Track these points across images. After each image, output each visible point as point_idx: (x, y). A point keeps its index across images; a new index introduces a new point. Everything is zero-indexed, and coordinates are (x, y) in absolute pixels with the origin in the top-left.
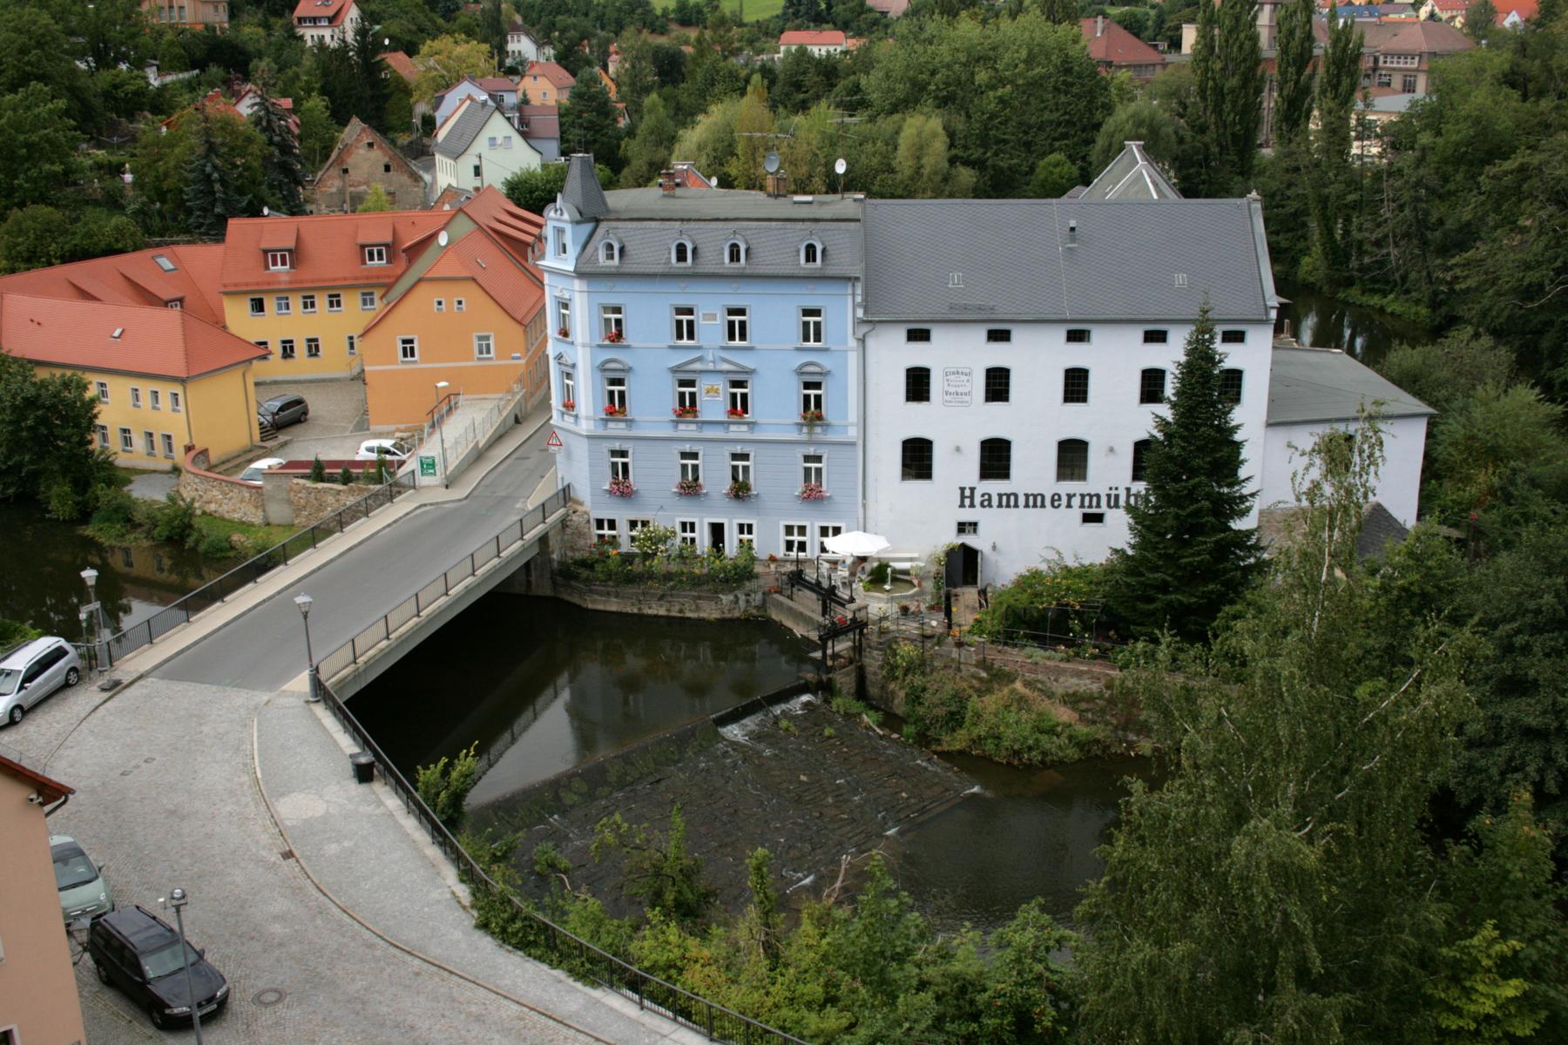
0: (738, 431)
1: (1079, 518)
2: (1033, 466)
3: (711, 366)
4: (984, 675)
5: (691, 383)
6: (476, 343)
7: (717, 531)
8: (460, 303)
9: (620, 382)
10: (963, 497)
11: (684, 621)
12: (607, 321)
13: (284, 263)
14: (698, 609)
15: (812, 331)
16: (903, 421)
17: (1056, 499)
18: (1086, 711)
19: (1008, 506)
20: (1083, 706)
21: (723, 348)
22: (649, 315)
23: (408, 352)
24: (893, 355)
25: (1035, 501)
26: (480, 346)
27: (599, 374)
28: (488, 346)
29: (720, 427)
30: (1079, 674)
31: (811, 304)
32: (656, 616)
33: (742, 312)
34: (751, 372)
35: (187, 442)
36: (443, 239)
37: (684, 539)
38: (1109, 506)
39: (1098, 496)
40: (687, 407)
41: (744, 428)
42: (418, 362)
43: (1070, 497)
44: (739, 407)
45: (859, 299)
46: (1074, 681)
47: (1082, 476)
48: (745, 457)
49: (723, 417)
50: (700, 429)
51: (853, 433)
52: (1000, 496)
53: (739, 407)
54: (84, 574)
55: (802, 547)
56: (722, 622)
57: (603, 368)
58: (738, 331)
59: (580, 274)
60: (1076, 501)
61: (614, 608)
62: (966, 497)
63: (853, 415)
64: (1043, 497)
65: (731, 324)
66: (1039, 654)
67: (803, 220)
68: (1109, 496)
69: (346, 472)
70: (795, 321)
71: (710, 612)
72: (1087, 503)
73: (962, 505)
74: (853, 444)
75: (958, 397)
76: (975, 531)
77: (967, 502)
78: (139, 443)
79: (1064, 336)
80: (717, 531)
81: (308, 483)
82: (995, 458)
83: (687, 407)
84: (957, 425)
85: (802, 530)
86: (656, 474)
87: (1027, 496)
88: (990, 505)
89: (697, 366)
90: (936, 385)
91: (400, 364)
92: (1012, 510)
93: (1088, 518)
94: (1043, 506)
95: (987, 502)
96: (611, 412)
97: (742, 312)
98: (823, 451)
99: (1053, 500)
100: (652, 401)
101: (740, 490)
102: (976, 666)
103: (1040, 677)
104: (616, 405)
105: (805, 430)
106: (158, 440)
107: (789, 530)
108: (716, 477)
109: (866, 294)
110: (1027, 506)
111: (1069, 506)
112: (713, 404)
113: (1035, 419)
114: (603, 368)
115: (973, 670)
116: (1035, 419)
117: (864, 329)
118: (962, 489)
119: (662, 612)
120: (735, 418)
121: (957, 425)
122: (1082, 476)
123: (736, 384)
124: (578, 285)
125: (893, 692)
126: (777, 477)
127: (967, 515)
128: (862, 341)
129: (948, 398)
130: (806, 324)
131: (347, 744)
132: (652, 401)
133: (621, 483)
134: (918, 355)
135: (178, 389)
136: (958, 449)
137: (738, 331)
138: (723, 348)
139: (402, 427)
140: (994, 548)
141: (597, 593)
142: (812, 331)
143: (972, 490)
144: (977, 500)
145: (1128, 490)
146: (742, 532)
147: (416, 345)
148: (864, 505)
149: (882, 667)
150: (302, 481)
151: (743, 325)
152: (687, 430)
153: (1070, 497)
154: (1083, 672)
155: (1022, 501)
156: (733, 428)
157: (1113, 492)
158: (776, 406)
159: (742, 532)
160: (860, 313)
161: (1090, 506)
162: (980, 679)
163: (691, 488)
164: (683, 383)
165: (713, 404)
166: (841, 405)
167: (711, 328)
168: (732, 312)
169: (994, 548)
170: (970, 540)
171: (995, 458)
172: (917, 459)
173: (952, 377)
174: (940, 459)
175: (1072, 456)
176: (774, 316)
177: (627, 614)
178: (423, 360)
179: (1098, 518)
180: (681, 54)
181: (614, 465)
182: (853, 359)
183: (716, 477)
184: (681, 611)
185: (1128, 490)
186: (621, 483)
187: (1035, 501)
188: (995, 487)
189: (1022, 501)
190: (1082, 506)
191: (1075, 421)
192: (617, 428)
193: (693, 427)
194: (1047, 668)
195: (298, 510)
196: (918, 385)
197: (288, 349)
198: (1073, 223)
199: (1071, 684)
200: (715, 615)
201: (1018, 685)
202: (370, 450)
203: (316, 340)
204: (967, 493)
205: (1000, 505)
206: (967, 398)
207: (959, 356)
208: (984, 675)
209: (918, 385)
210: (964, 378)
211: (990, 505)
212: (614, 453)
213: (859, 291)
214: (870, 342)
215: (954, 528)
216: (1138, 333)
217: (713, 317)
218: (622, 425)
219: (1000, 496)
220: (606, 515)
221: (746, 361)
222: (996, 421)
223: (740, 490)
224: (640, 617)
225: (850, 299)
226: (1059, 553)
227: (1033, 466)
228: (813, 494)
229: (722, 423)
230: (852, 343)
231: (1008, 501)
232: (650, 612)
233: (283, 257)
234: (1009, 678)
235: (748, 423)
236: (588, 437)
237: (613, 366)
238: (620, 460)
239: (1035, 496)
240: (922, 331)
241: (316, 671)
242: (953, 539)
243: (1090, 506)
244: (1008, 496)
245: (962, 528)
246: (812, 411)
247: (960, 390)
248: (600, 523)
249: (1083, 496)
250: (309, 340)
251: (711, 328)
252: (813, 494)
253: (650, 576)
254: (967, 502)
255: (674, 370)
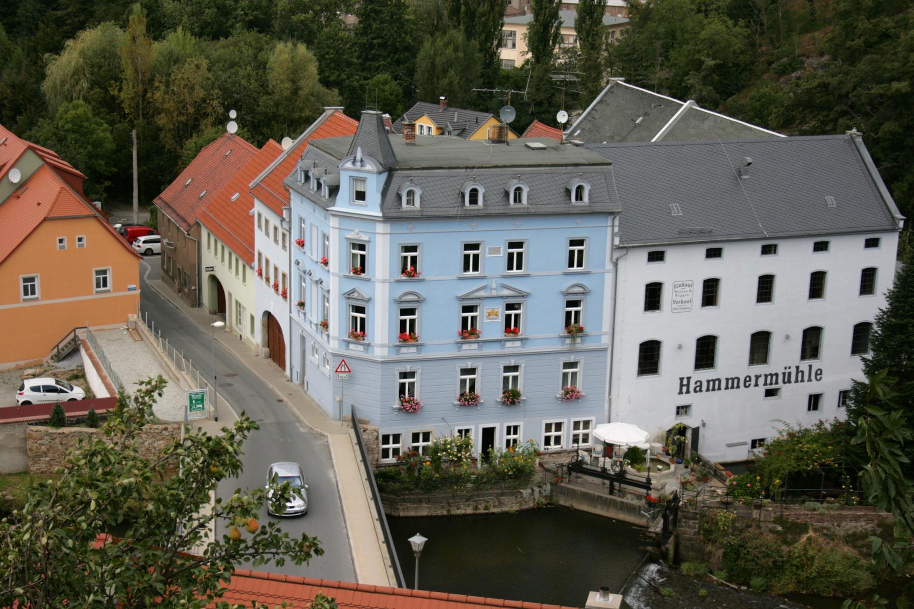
0: (513, 346)
1: (763, 393)
2: (732, 357)
3: (494, 293)
4: (780, 528)
7: (488, 435)
10: (682, 385)
11: (489, 516)
12: (354, 255)
14: (501, 504)
15: (575, 259)
16: (639, 326)
17: (748, 379)
18: (862, 546)
20: (860, 543)
21: (505, 277)
22: (441, 249)
23: (29, 290)
24: (638, 272)
25: (733, 383)
26: (98, 280)
27: (344, 301)
29: (498, 345)
30: (856, 519)
32: (465, 516)
34: (525, 295)
38: (784, 382)
40: (468, 329)
41: (518, 344)
43: (757, 377)
44: (511, 326)
45: (616, 229)
46: (853, 524)
50: (480, 348)
53: (511, 326)
55: (558, 440)
56: (522, 513)
57: (348, 295)
58: (514, 261)
59: (386, 219)
60: (761, 381)
61: (424, 513)
62: (684, 385)
63: (606, 327)
66: (821, 507)
67: (566, 165)
68: (784, 374)
69: (92, 414)
71: (511, 505)
72: (769, 382)
73: (681, 393)
74: (605, 350)
75: (681, 305)
77: (684, 389)
80: (488, 435)
81: (52, 430)
82: (706, 351)
83: (468, 329)
85: (559, 426)
86: (437, 390)
88: (701, 391)
89: (482, 294)
92: (716, 392)
93: (770, 393)
95: (699, 389)
96: (354, 335)
99: (745, 381)
100: (438, 325)
101: (512, 398)
102: (774, 522)
103: (826, 524)
104: (407, 332)
105: (568, 341)
108: (490, 387)
112: (490, 324)
114: (348, 295)
115: (771, 525)
117: (617, 254)
118: (682, 379)
119: (469, 511)
120: (511, 336)
121: (677, 328)
123: (509, 307)
124: (380, 228)
125: (710, 553)
126: (539, 384)
127: (684, 400)
129: (675, 306)
132: (438, 325)
133: (408, 403)
136: (680, 347)
137: (514, 261)
138: (505, 277)
141: (410, 501)
142: (575, 259)
143: (689, 379)
145: (797, 367)
147: (37, 283)
149: (698, 533)
150: (40, 428)
152: (470, 349)
153: (757, 377)
154: (860, 516)
156: (508, 344)
157: (787, 371)
158: (543, 322)
159: (508, 433)
160: (617, 241)
161: (771, 384)
162: (777, 532)
163: (469, 398)
165: (490, 324)
167: (493, 259)
170: (686, 421)
171: (706, 351)
172: (649, 357)
173: (679, 289)
176: (546, 244)
177: (437, 517)
178: (44, 297)
182: (609, 278)
183: (490, 387)
184: (486, 508)
185: (797, 367)
186: (408, 403)
187: (733, 383)
188: (705, 375)
190: (765, 384)
192: (409, 352)
193: (475, 346)
194: (832, 516)
195: (37, 457)
198: (749, 160)
199: (851, 526)
200: (515, 508)
201: (811, 533)
202: (35, 389)
206: (688, 305)
207: (684, 269)
208: (780, 528)
209: (653, 296)
210: (688, 289)
211: (701, 391)
213: (617, 223)
214: (621, 264)
215: (674, 410)
217: (497, 250)
218: (414, 350)
220: (391, 431)
221: (522, 286)
223: (512, 398)
224: (450, 518)
225: (609, 230)
226: (785, 423)
227: (732, 357)
228: (570, 395)
229: (500, 341)
230: (609, 266)
231: (714, 385)
232: (458, 512)
234: (804, 528)
235: (521, 340)
236: (383, 363)
242: (671, 421)
243: (771, 384)
246: (573, 326)
247: (684, 299)
248: (386, 439)
249: (766, 376)
251: (493, 259)
252: (570, 395)
253: (459, 479)
255: (462, 299)
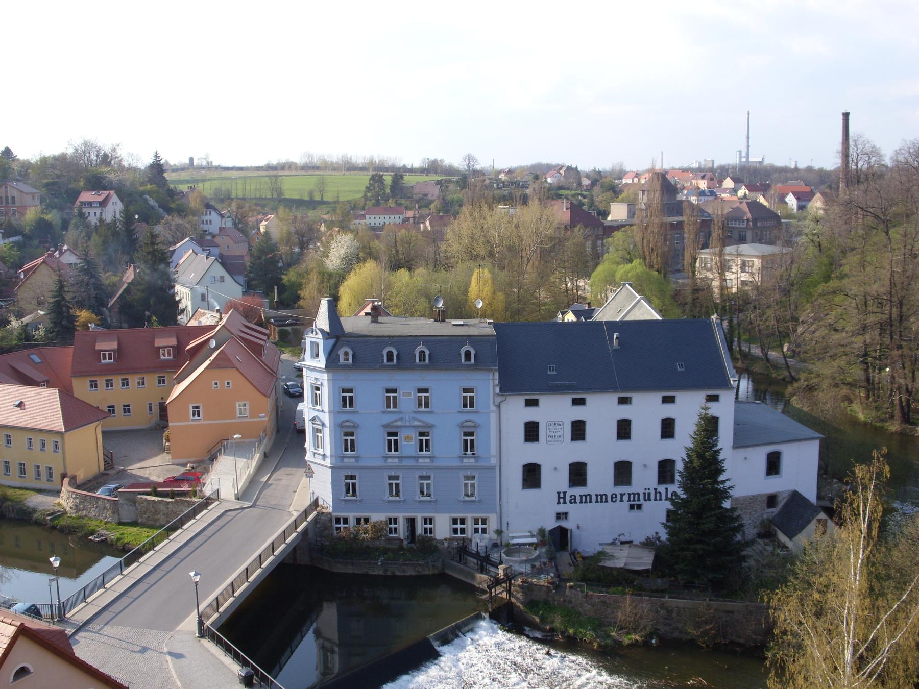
2: (600, 478)
3: (408, 424)
5: (395, 434)
6: (191, 410)
7: (412, 522)
8: (228, 383)
10: (559, 498)
13: (110, 359)
15: (468, 403)
16: (521, 453)
17: (613, 497)
19: (586, 502)
25: (601, 498)
28: (198, 412)
31: (467, 385)
33: (350, 391)
35: (62, 471)
37: (426, 529)
38: (645, 500)
39: (638, 494)
40: (393, 446)
43: (622, 495)
44: (423, 446)
45: (497, 382)
51: (494, 461)
52: (581, 496)
53: (423, 446)
54: (52, 559)
55: (463, 531)
60: (626, 498)
61: (350, 571)
62: (561, 498)
63: (494, 451)
64: (606, 496)
65: (344, 399)
68: (644, 494)
70: (381, 396)
73: (559, 503)
74: (494, 468)
75: (555, 439)
76: (566, 518)
77: (562, 500)
78: (31, 472)
79: (523, 403)
80: (412, 522)
82: (578, 473)
83: (393, 446)
84: (555, 455)
85: (463, 521)
86: (373, 487)
87: (597, 496)
88: (575, 502)
89: (399, 423)
90: (542, 432)
91: (192, 421)
93: (632, 507)
94: (606, 501)
95: (573, 500)
97: (350, 391)
98: (400, 474)
99: (612, 498)
107: (455, 521)
110: (581, 502)
111: (622, 501)
112: (409, 446)
113: (600, 450)
116: (600, 450)
118: (559, 493)
121: (555, 455)
123: (422, 434)
127: (562, 508)
130: (388, 398)
132: (371, 443)
135: (58, 439)
136: (555, 469)
139: (192, 460)
140: (578, 527)
142: (468, 403)
143: (565, 493)
144: (568, 499)
145: (656, 489)
146: (426, 523)
147: (201, 410)
148: (500, 505)
151: (351, 398)
153: (622, 495)
157: (647, 491)
158: (447, 444)
159: (426, 523)
161: (634, 500)
164: (390, 434)
165: (409, 446)
166: (487, 443)
169: (578, 527)
171: (578, 473)
174: (545, 476)
175: (623, 471)
179: (639, 507)
182: (493, 417)
185: (656, 489)
187: (601, 498)
188: (578, 491)
190: (629, 500)
203: (129, 406)
204: (562, 495)
205: (581, 502)
209: (532, 432)
210: (559, 427)
211: (575, 502)
212: (347, 477)
214: (503, 406)
215: (554, 516)
219: (581, 496)
220: (341, 514)
221: (429, 419)
225: (491, 382)
227: (600, 478)
229: (414, 457)
230: (493, 408)
231: (586, 499)
233: (110, 355)
237: (348, 424)
238: (351, 482)
239: (602, 496)
240: (627, 398)
243: (634, 500)
244: (586, 496)
245: (559, 516)
249: (629, 494)
250: (124, 406)
254: (562, 500)
255: (385, 426)
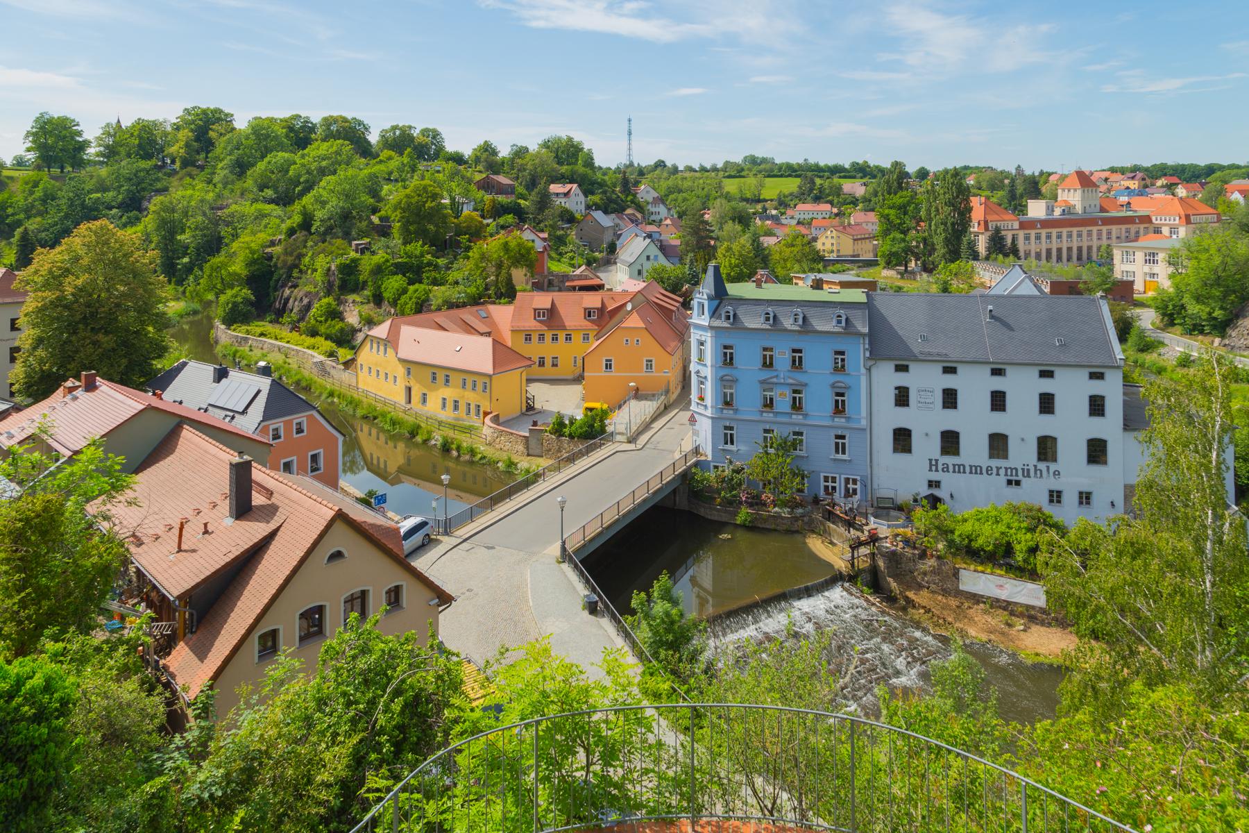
1: (1005, 483)
2: (974, 449)
9: (842, 395)
10: (931, 465)
16: (889, 418)
17: (989, 469)
24: (886, 379)
25: (976, 470)
36: (629, 307)
42: (613, 373)
43: (998, 469)
47: (1006, 457)
48: (843, 437)
49: (789, 410)
51: (864, 423)
53: (797, 406)
57: (833, 386)
58: (797, 364)
60: (1002, 472)
62: (933, 465)
63: (864, 413)
70: (830, 358)
73: (931, 470)
74: (864, 430)
82: (950, 441)
89: (775, 380)
90: (939, 398)
93: (1009, 482)
95: (946, 469)
106: (472, 407)
109: (870, 343)
111: (998, 474)
121: (927, 422)
122: (1006, 457)
127: (934, 476)
128: (869, 370)
131: (582, 590)
134: (902, 379)
137: (797, 364)
140: (952, 496)
143: (937, 461)
144: (940, 467)
155: (968, 469)
158: (819, 403)
166: (858, 406)
168: (794, 351)
171: (950, 441)
175: (998, 444)
179: (1018, 483)
180: (270, 257)
181: (726, 435)
187: (976, 470)
188: (950, 460)
189: (968, 469)
191: (999, 423)
196: (902, 397)
197: (542, 364)
198: (990, 307)
209: (902, 397)
212: (726, 428)
214: (874, 371)
216: (1085, 373)
222: (950, 420)
227: (974, 449)
230: (863, 370)
231: (959, 469)
241: (564, 543)
